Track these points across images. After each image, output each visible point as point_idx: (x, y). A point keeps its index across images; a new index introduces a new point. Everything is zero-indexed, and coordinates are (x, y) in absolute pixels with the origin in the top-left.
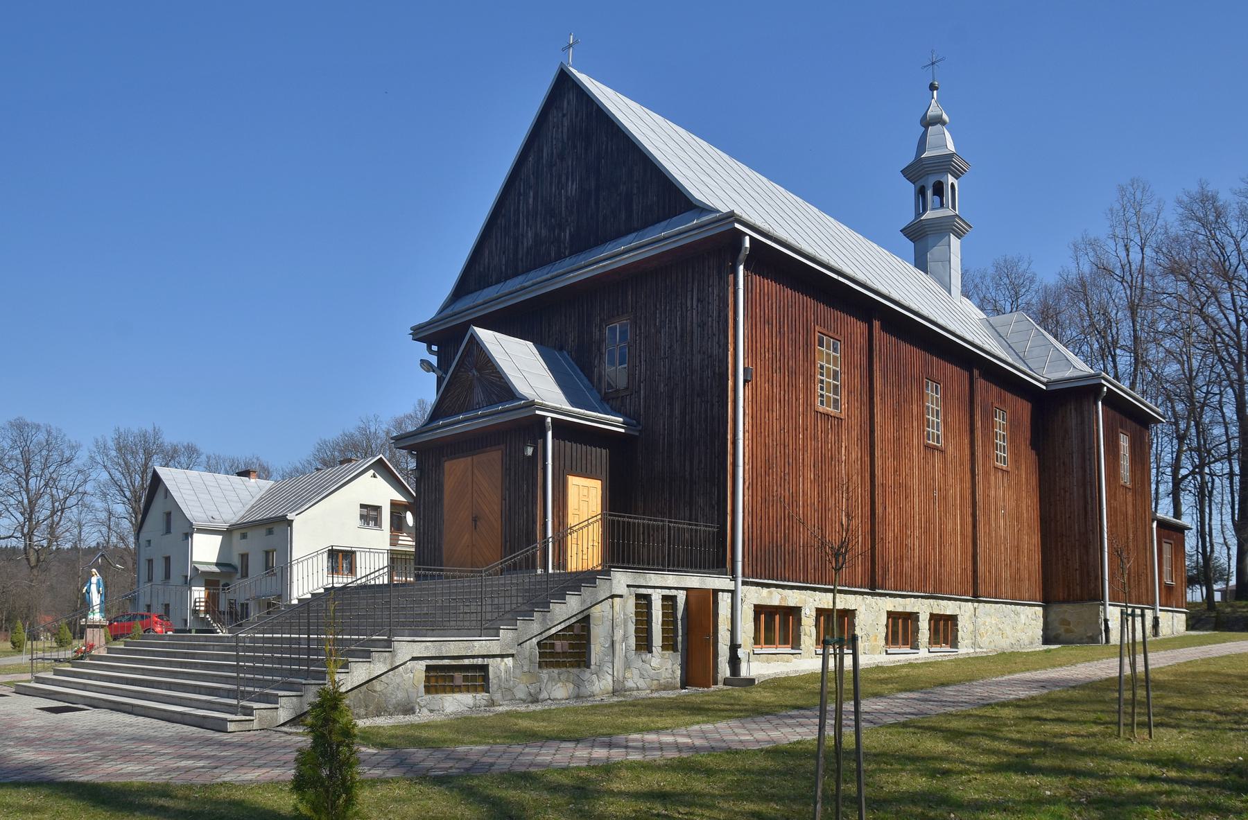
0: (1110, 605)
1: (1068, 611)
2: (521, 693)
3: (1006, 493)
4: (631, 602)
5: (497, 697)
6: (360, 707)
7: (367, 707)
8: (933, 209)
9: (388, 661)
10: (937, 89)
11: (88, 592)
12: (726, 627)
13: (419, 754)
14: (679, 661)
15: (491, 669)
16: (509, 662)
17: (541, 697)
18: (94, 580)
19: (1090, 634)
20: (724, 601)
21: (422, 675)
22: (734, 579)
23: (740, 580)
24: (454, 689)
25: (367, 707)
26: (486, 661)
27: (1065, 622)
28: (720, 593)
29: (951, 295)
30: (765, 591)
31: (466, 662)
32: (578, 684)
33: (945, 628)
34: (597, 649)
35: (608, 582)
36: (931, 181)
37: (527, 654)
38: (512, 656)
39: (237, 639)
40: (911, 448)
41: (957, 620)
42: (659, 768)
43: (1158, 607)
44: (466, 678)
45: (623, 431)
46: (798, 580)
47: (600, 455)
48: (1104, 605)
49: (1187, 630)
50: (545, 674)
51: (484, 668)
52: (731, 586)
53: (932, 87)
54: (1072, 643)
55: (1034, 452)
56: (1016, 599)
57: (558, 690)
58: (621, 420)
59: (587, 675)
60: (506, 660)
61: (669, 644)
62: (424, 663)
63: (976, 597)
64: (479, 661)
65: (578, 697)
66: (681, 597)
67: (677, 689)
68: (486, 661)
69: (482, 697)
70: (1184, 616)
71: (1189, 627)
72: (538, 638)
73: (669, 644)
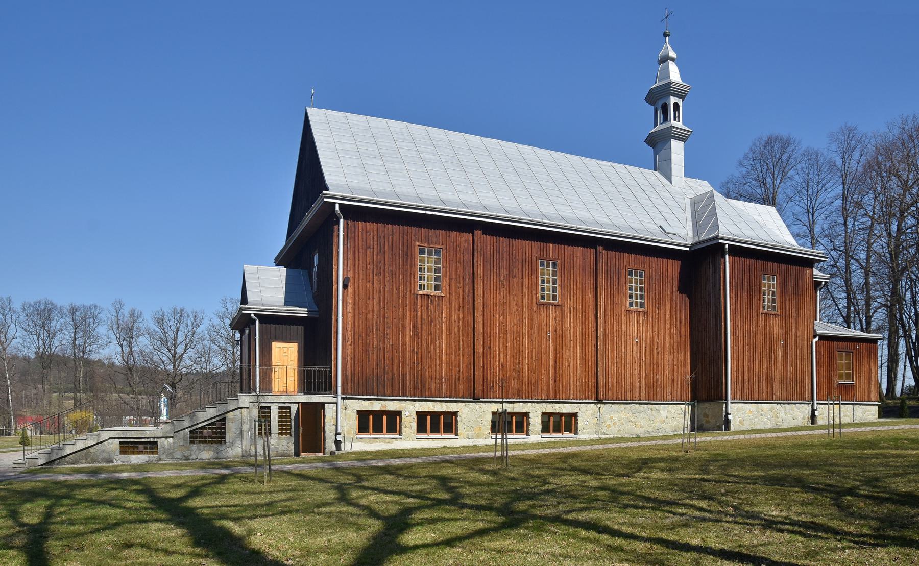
0: (731, 403)
1: (707, 407)
2: (178, 455)
3: (643, 329)
4: (255, 413)
5: (163, 457)
6: (83, 459)
7: (86, 459)
8: (661, 124)
9: (96, 439)
10: (669, 35)
11: (160, 405)
12: (332, 423)
13: (647, 557)
14: (293, 441)
15: (158, 443)
16: (171, 440)
17: (191, 458)
18: (163, 399)
19: (718, 424)
20: (330, 411)
21: (118, 446)
22: (337, 397)
23: (340, 397)
24: (139, 453)
25: (86, 459)
26: (155, 440)
27: (706, 416)
28: (326, 405)
29: (671, 183)
30: (367, 402)
31: (143, 440)
32: (218, 452)
33: (568, 422)
34: (229, 437)
35: (236, 401)
36: (660, 103)
37: (182, 437)
38: (172, 437)
39: (506, 447)
40: (440, 323)
41: (577, 416)
42: (460, 519)
43: (816, 402)
44: (145, 448)
45: (306, 315)
46: (394, 394)
47: (301, 329)
48: (727, 404)
49: (880, 417)
50: (194, 447)
51: (156, 443)
52: (335, 400)
53: (665, 35)
54: (708, 430)
55: (685, 298)
56: (674, 400)
57: (206, 454)
58: (306, 309)
59: (224, 447)
60: (168, 439)
61: (284, 430)
62: (118, 441)
63: (599, 401)
64: (152, 440)
65: (217, 458)
66: (294, 408)
67: (292, 456)
68: (155, 440)
69: (154, 457)
70: (876, 407)
71: (881, 415)
72: (190, 429)
73: (284, 431)
